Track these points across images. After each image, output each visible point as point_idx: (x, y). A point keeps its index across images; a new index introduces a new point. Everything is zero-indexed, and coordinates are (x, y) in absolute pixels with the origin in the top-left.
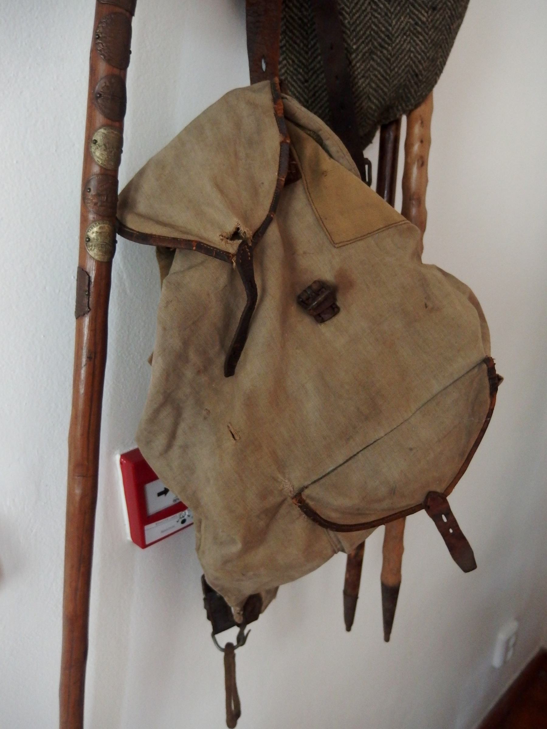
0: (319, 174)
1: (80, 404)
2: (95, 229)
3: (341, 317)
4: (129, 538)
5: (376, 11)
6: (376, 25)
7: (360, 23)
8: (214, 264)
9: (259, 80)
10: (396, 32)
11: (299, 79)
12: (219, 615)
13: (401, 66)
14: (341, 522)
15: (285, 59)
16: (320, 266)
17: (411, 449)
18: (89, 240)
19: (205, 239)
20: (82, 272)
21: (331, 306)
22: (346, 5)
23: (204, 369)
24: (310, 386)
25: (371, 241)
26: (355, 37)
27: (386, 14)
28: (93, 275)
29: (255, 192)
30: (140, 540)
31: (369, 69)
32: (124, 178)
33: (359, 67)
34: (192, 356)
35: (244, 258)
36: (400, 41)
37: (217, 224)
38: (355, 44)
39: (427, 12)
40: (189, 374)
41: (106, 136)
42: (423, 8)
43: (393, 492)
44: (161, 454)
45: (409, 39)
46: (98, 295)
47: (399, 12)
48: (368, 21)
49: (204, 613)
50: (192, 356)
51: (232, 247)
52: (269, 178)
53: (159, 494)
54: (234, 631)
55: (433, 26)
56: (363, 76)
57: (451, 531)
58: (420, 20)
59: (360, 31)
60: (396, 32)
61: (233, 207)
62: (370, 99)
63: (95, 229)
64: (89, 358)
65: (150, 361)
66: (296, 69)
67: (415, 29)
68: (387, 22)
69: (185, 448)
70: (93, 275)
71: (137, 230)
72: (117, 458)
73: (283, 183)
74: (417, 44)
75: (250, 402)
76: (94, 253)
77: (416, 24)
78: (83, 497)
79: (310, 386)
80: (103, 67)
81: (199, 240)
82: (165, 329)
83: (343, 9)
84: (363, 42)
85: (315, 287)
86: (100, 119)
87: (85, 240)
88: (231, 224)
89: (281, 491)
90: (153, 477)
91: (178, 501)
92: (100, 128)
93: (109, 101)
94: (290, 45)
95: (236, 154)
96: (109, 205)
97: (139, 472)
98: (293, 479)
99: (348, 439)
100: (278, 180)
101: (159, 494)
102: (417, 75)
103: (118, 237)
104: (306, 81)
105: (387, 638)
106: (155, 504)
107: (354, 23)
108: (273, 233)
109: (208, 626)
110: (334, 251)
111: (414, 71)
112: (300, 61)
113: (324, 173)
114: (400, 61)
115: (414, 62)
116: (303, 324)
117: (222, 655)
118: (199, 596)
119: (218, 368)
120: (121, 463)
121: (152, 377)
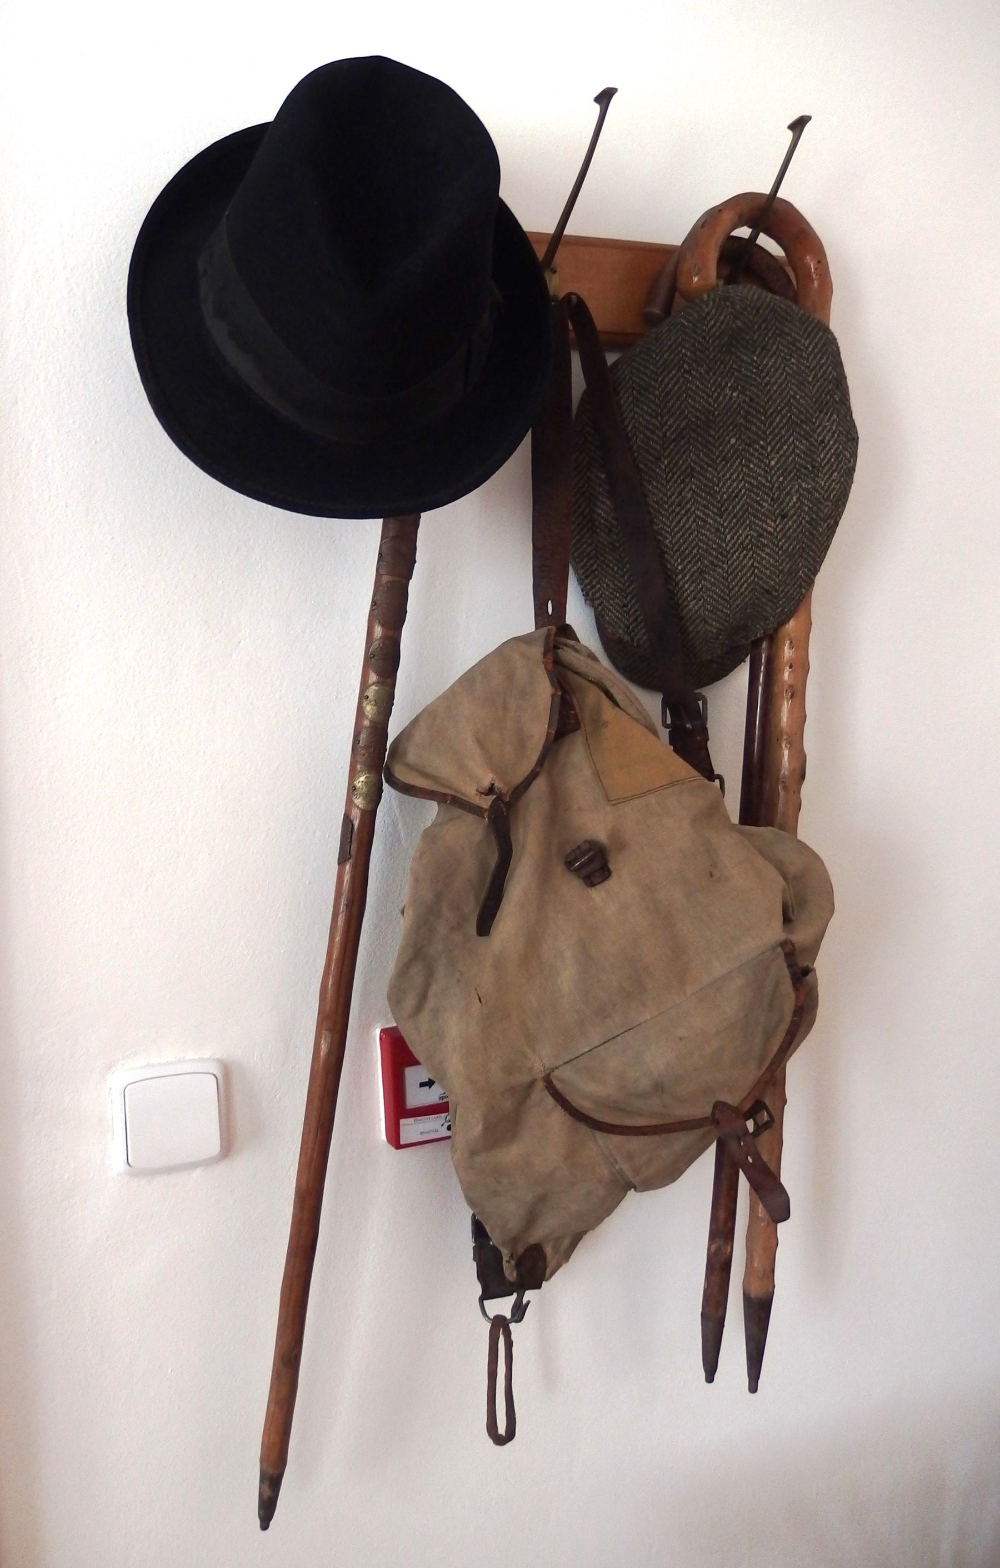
0: (598, 724)
2: (362, 779)
3: (612, 883)
4: (384, 1137)
5: (703, 527)
6: (704, 543)
7: (684, 542)
8: (470, 818)
9: (543, 626)
10: (731, 548)
11: (617, 604)
12: (492, 1281)
13: (743, 584)
14: (597, 1116)
15: (598, 583)
16: (594, 824)
17: (681, 1039)
18: (355, 788)
19: (463, 794)
20: (347, 820)
21: (601, 868)
22: (666, 524)
23: (457, 927)
24: (568, 954)
25: (652, 799)
26: (680, 556)
27: (718, 530)
28: (356, 823)
29: (521, 743)
30: (395, 1139)
31: (701, 589)
32: (394, 730)
33: (687, 587)
34: (446, 912)
35: (501, 815)
36: (739, 557)
37: (474, 778)
38: (680, 564)
39: (775, 522)
40: (442, 929)
41: (377, 692)
42: (768, 517)
43: (659, 1088)
44: (410, 1016)
45: (751, 553)
46: (360, 845)
47: (736, 524)
48: (694, 539)
49: (472, 1267)
50: (446, 912)
51: (486, 803)
52: (538, 729)
53: (422, 1085)
54: (510, 1300)
55: (783, 536)
56: (695, 598)
57: (750, 1160)
58: (766, 530)
59: (685, 550)
60: (731, 548)
61: (491, 762)
62: (706, 622)
63: (362, 779)
64: (347, 905)
65: (403, 913)
66: (612, 593)
67: (759, 541)
68: (720, 538)
69: (436, 1012)
70: (356, 823)
71: (402, 779)
72: (378, 1032)
73: (553, 736)
74: (763, 558)
75: (499, 965)
77: (760, 535)
78: (329, 1053)
79: (568, 954)
81: (454, 794)
82: (416, 880)
83: (662, 529)
84: (690, 562)
85: (584, 847)
86: (373, 678)
87: (352, 789)
88: (487, 779)
89: (531, 1069)
90: (414, 1062)
91: (445, 1100)
92: (372, 684)
93: (384, 659)
94: (603, 569)
95: (505, 708)
96: (377, 756)
97: (398, 1054)
98: (542, 1058)
99: (605, 1018)
100: (548, 733)
101: (422, 1085)
102: (768, 592)
103: (385, 786)
104: (625, 606)
105: (753, 1388)
106: (416, 1097)
107: (676, 543)
108: (539, 787)
109: (478, 1290)
110: (608, 808)
111: (763, 588)
112: (616, 586)
113: (605, 724)
114: (741, 579)
115: (761, 579)
116: (570, 887)
117: (488, 1326)
118: (467, 1243)
119: (472, 928)
120: (381, 1039)
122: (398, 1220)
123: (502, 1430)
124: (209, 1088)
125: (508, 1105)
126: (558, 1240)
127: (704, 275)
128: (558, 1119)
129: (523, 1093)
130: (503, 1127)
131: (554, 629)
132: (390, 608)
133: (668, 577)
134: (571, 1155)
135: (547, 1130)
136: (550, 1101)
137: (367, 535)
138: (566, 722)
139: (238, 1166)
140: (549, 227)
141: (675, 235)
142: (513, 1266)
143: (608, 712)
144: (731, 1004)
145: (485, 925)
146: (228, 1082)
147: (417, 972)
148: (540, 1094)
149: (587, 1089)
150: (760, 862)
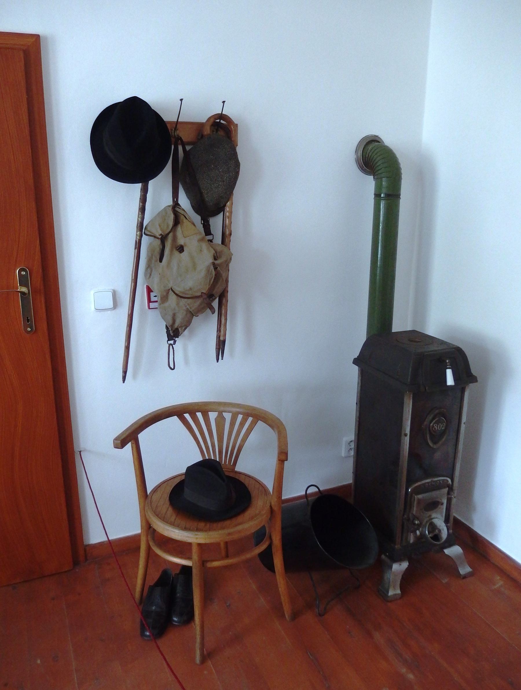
1: (460, 462)
12: (170, 338)
16: (181, 241)
29: (168, 226)
32: (145, 225)
35: (163, 239)
37: (158, 232)
43: (191, 289)
51: (160, 237)
52: (171, 223)
61: (161, 230)
76: (138, 238)
80: (141, 204)
88: (160, 232)
93: (142, 210)
106: (153, 299)
108: (171, 235)
116: (176, 253)
121: (410, 369)
122: (152, 327)
123: (172, 367)
124: (110, 295)
125: (165, 294)
126: (181, 327)
127: (207, 131)
128: (174, 296)
129: (168, 292)
130: (164, 298)
131: (176, 204)
132: (143, 200)
133: (201, 193)
134: (178, 304)
135: (172, 298)
136: (173, 293)
137: (139, 186)
138: (177, 222)
139: (117, 311)
140: (176, 120)
141: (204, 120)
142: (173, 334)
143: (185, 220)
144: (203, 273)
145: (161, 261)
146: (115, 294)
147: (149, 270)
148: (171, 292)
149: (177, 290)
150: (211, 248)
